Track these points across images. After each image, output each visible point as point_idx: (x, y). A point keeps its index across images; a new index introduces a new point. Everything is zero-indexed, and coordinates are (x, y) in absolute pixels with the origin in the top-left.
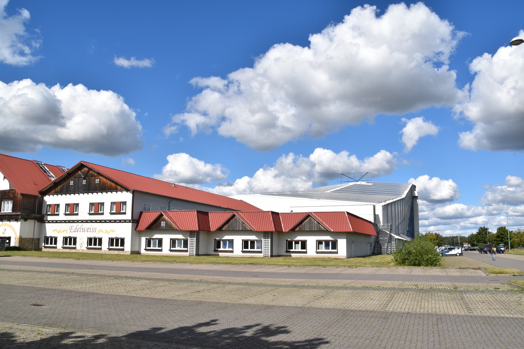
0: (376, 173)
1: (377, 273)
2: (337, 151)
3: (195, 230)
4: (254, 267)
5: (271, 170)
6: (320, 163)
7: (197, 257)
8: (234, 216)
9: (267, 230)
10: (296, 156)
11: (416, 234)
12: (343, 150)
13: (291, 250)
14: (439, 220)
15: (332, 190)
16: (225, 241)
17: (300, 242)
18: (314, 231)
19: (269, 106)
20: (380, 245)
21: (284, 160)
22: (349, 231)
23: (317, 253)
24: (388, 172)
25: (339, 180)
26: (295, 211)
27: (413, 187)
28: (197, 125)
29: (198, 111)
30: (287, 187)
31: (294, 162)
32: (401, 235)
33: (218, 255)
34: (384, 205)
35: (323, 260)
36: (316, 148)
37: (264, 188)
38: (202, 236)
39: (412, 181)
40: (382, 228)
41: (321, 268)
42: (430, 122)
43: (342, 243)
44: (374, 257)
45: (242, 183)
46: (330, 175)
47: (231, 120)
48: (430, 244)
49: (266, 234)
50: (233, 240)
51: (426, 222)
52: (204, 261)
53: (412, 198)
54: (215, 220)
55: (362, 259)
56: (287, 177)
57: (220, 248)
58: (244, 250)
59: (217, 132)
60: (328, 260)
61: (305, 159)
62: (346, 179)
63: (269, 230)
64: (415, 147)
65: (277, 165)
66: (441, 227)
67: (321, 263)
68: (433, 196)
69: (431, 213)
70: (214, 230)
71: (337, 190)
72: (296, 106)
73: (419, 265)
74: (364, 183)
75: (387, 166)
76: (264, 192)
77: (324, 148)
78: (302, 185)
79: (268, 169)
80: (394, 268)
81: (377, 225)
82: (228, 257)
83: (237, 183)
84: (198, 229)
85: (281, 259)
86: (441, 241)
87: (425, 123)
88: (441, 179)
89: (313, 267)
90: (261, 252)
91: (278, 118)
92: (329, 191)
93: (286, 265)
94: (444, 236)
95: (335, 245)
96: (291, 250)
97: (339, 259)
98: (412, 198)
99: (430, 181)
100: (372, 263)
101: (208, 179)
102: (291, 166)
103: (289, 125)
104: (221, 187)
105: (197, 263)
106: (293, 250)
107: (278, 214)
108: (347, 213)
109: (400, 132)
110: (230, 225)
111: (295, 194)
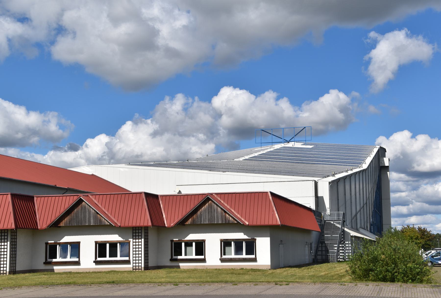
0: (321, 127)
1: (323, 293)
2: (256, 90)
3: (9, 227)
4: (116, 287)
5: (146, 123)
6: (230, 111)
7: (12, 276)
8: (81, 201)
9: (138, 225)
10: (188, 99)
11: (385, 228)
12: (267, 90)
13: (179, 257)
14: (426, 206)
15: (247, 157)
16: (64, 246)
17: (194, 244)
18: (218, 224)
19: (144, 10)
20: (326, 247)
21: (167, 106)
22: (274, 223)
23: (222, 260)
24: (340, 126)
25: (258, 140)
26: (185, 191)
27: (382, 152)
28: (9, 40)
29: (8, 11)
30: (174, 152)
31: (186, 109)
32: (361, 230)
33: (53, 270)
34: (333, 182)
35: (232, 273)
36: (222, 87)
37: (135, 154)
38: (21, 239)
39: (382, 141)
40: (328, 218)
41: (230, 287)
42: (420, 37)
43: (263, 244)
44: (317, 267)
45: (96, 145)
46: (245, 132)
47: (74, 33)
48: (411, 247)
49: (136, 231)
50: (79, 243)
51: (404, 210)
52: (24, 282)
53: (379, 169)
54: (47, 210)
55: (297, 270)
56: (175, 135)
57: (56, 258)
58: (99, 259)
59: (49, 54)
60: (241, 272)
61: (204, 105)
62: (269, 138)
63: (142, 224)
64: (390, 83)
65: (157, 115)
66: (429, 217)
67: (228, 278)
68: (419, 165)
69: (414, 194)
70: (45, 226)
71: (255, 157)
72: (188, 12)
73: (393, 280)
74: (298, 145)
75: (341, 116)
76: (134, 161)
77: (235, 87)
78: (199, 149)
79: (141, 122)
80: (350, 285)
81: (321, 214)
82: (70, 273)
83: (87, 146)
84: (13, 227)
85: (162, 273)
86: (430, 240)
87: (410, 41)
88: (432, 136)
89: (216, 284)
90: (128, 262)
91: (158, 31)
92: (241, 159)
93: (170, 282)
94: (435, 233)
95: (251, 247)
96: (179, 257)
97: (259, 270)
98: (379, 169)
99: (414, 140)
100: (313, 276)
101: (35, 140)
102: (179, 117)
103: (176, 45)
104: (59, 153)
105: (11, 287)
106: (183, 257)
107: (156, 197)
108: (272, 194)
109: (366, 58)
110: (73, 219)
111: (185, 163)
